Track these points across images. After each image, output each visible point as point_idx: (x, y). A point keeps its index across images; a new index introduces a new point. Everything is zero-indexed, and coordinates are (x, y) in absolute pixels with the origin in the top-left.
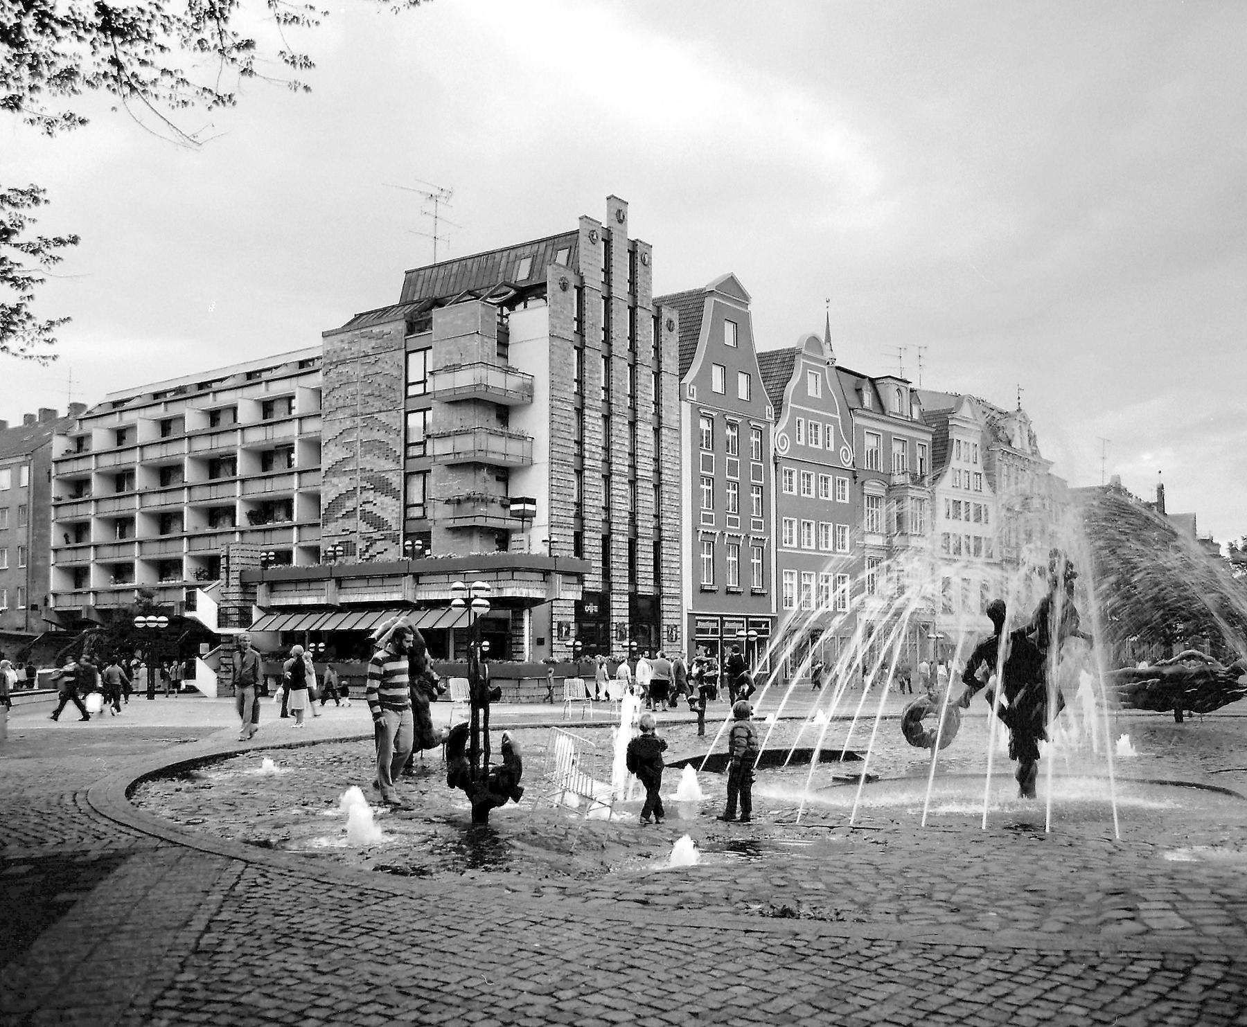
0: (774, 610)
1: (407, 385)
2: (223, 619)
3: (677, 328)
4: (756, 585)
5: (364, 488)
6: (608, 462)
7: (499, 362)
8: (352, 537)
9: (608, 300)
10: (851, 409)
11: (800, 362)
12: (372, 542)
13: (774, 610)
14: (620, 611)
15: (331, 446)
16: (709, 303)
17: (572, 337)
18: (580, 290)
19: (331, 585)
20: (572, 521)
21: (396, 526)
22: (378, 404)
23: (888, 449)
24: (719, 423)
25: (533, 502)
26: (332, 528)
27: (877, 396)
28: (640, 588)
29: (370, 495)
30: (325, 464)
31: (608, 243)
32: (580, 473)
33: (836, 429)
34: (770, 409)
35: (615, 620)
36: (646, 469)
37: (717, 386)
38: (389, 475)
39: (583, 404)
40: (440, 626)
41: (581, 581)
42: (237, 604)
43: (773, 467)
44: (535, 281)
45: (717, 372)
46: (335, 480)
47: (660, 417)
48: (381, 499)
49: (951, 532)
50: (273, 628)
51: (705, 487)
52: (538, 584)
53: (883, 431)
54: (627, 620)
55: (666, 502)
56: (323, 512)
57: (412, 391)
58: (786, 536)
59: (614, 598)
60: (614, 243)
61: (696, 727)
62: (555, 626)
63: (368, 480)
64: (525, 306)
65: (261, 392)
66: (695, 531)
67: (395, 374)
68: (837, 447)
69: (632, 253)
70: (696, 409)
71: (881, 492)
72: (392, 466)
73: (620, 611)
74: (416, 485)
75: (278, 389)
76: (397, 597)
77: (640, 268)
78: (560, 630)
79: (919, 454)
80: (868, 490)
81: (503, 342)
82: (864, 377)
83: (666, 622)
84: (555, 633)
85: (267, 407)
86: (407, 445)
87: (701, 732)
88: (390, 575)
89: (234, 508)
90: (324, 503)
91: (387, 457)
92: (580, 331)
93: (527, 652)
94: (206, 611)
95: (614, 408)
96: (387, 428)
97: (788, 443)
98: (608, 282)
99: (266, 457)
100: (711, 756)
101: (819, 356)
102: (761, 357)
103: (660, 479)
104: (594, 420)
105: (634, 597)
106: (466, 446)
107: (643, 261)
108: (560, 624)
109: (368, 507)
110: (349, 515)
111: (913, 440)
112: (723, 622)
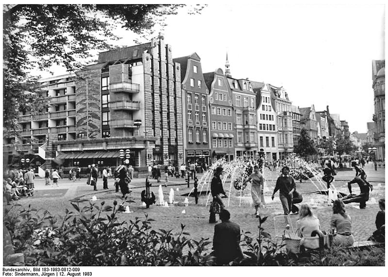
0: (210, 147)
1: (102, 87)
2: (47, 154)
3: (180, 68)
4: (205, 141)
5: (89, 117)
6: (161, 108)
7: (129, 81)
8: (85, 131)
9: (160, 62)
10: (231, 89)
11: (216, 76)
12: (92, 132)
13: (210, 147)
14: (166, 150)
15: (79, 104)
16: (189, 60)
17: (150, 73)
18: (152, 59)
19: (80, 145)
20: (151, 125)
21: (100, 128)
22: (93, 93)
23: (243, 100)
24: (193, 95)
25: (140, 121)
26: (80, 128)
27: (239, 85)
28: (171, 143)
29: (91, 119)
30: (77, 109)
31: (159, 46)
32: (154, 128)
33: (227, 96)
34: (207, 90)
35: (164, 153)
36: (172, 110)
37: (192, 85)
38: (97, 113)
39: (153, 92)
40: (114, 157)
41: (154, 142)
42: (51, 151)
43: (209, 107)
44: (139, 57)
45: (192, 80)
46: (80, 114)
47: (176, 95)
48: (94, 120)
49: (262, 123)
50: (63, 158)
51: (189, 113)
52: (142, 144)
53: (241, 95)
54: (167, 153)
55: (178, 118)
56: (76, 123)
57: (104, 89)
58: (213, 127)
59: (164, 146)
60: (161, 46)
61: (187, 185)
62: (147, 155)
63: (91, 114)
64: (136, 65)
65: (56, 87)
66: (187, 126)
67: (98, 84)
68: (228, 100)
69: (166, 48)
70: (186, 91)
71: (241, 113)
72: (97, 110)
73: (166, 150)
74: (105, 115)
75: (60, 86)
76: (101, 148)
77: (169, 52)
78: (149, 156)
79: (252, 102)
80: (237, 112)
81: (130, 74)
82: (235, 79)
83: (179, 153)
84: (147, 157)
85: (57, 91)
86: (102, 104)
87: (188, 187)
88: (98, 142)
89: (47, 121)
90: (77, 120)
91: (96, 108)
92: (152, 71)
93: (139, 164)
94: (42, 153)
95: (163, 93)
96: (96, 100)
97: (213, 100)
98: (160, 57)
99: (57, 107)
100: (191, 193)
101: (221, 74)
102: (204, 74)
103: (176, 112)
104: (157, 96)
105: (170, 146)
106: (119, 105)
107: (170, 50)
108: (148, 155)
109: (91, 122)
110: (85, 124)
111: (250, 97)
112: (196, 152)
